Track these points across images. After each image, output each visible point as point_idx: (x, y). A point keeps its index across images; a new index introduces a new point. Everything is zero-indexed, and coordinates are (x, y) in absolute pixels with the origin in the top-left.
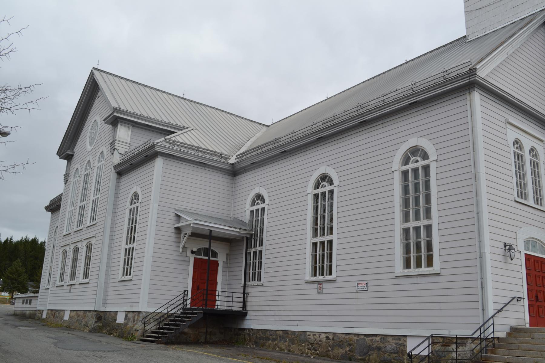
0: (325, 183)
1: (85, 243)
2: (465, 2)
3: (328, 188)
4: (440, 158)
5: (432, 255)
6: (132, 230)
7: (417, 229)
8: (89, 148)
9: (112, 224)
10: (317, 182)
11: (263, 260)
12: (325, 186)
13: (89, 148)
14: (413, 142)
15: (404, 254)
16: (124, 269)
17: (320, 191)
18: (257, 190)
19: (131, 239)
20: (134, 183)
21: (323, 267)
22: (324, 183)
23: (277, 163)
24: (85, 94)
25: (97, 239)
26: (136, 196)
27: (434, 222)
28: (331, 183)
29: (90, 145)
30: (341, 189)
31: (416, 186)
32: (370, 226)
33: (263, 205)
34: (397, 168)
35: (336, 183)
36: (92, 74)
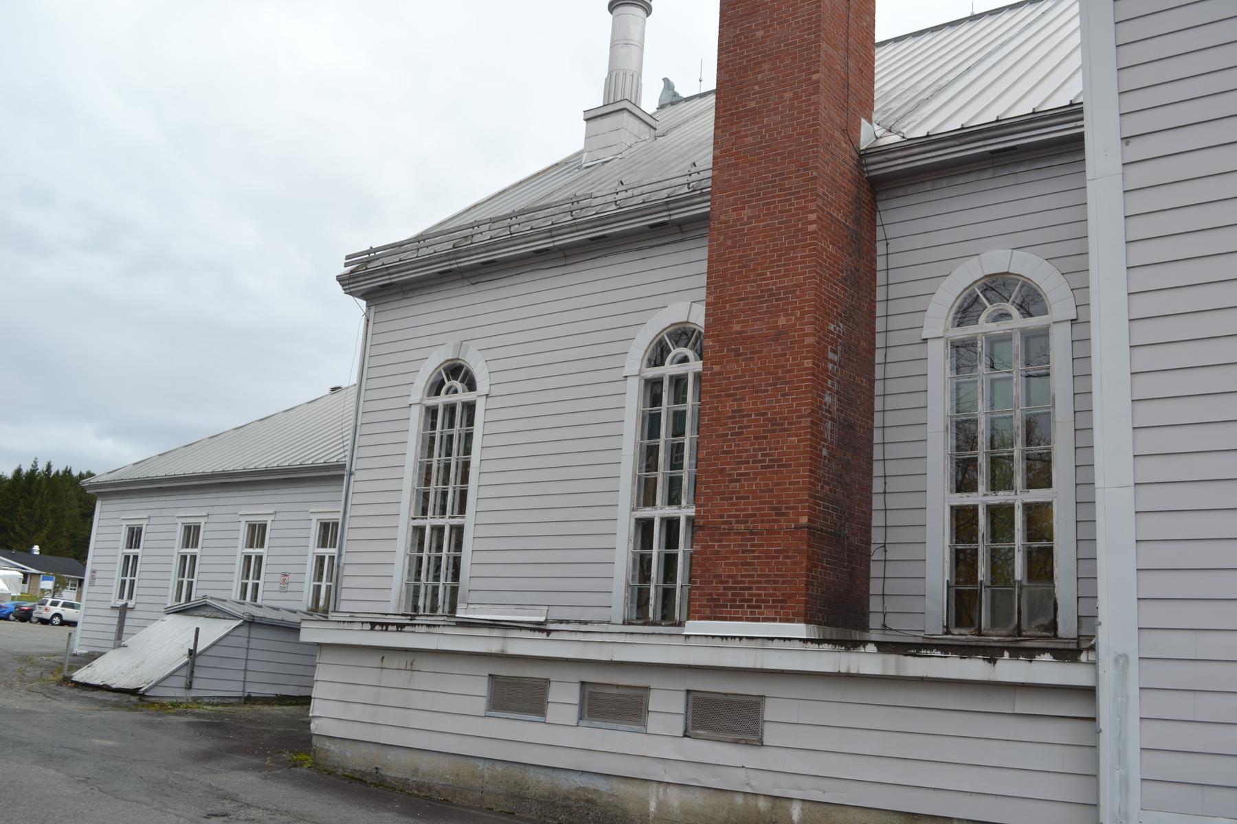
2: (612, 8)
3: (463, 396)
4: (496, 391)
7: (440, 529)
12: (456, 392)
14: (996, 260)
17: (442, 400)
27: (468, 521)
28: (471, 386)
30: (493, 403)
35: (482, 386)
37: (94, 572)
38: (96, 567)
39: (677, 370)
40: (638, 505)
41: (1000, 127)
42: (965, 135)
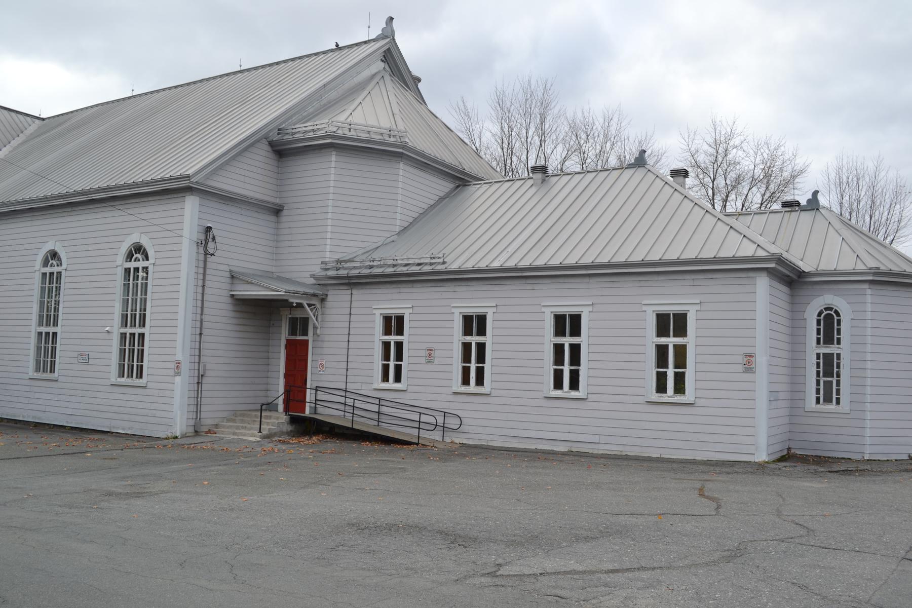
5: (684, 373)
11: (146, 348)
17: (132, 265)
33: (145, 264)
35: (151, 261)
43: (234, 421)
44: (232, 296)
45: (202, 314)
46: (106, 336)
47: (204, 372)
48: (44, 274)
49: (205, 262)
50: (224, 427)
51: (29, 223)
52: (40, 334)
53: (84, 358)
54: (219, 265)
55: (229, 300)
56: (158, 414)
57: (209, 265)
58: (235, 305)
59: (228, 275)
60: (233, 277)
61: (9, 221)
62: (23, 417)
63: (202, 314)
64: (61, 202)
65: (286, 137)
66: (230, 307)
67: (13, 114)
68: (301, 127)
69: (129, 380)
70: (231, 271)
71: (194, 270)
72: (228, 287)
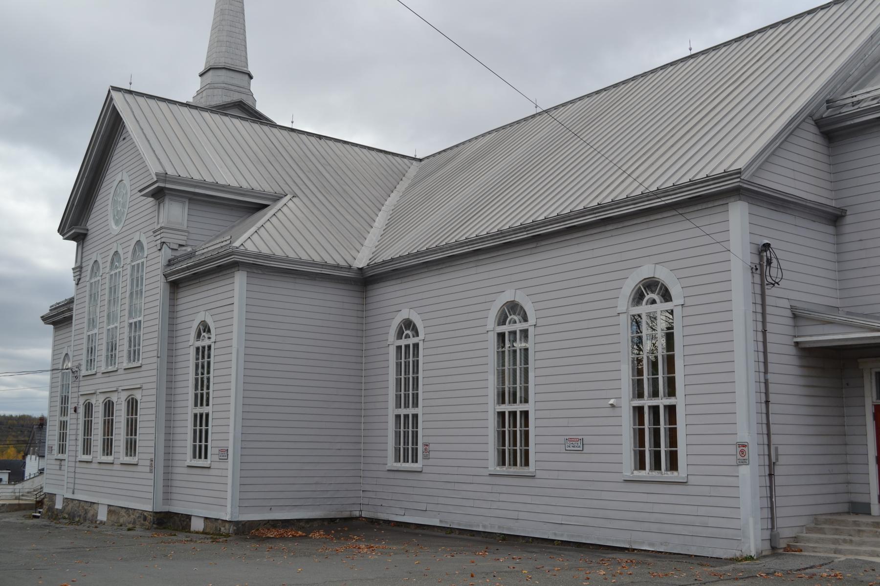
0: (516, 318)
1: (124, 396)
4: (689, 301)
5: (674, 377)
6: (202, 384)
7: (655, 410)
8: (115, 228)
9: (167, 453)
10: (501, 314)
12: (515, 322)
13: (115, 228)
14: (646, 272)
15: (635, 447)
16: (195, 431)
17: (403, 342)
18: (404, 314)
19: (202, 399)
20: (198, 305)
21: (515, 371)
22: (513, 316)
23: (437, 272)
24: (97, 138)
25: (145, 393)
26: (205, 328)
27: (679, 401)
29: (117, 223)
31: (656, 433)
32: (584, 396)
33: (524, 326)
34: (624, 309)
35: (532, 320)
36: (109, 100)
37: (426, 445)
38: (427, 440)
39: (512, 328)
40: (634, 397)
41: (501, 233)
42: (491, 237)
43: (821, 531)
44: (797, 343)
45: (766, 372)
46: (610, 412)
47: (777, 459)
48: (399, 348)
49: (763, 295)
50: (809, 540)
51: (473, 271)
52: (502, 415)
53: (576, 444)
54: (779, 300)
55: (792, 350)
56: (711, 522)
57: (769, 301)
58: (801, 357)
59: (788, 313)
60: (795, 316)
61: (415, 277)
62: (484, 526)
63: (766, 372)
64: (466, 249)
65: (844, 110)
66: (795, 361)
67: (390, 157)
68: (861, 94)
69: (655, 474)
70: (792, 308)
71: (751, 308)
72: (790, 331)
